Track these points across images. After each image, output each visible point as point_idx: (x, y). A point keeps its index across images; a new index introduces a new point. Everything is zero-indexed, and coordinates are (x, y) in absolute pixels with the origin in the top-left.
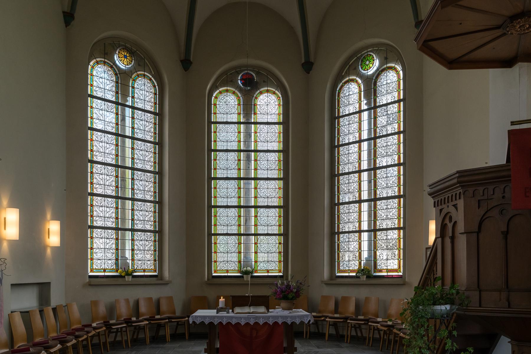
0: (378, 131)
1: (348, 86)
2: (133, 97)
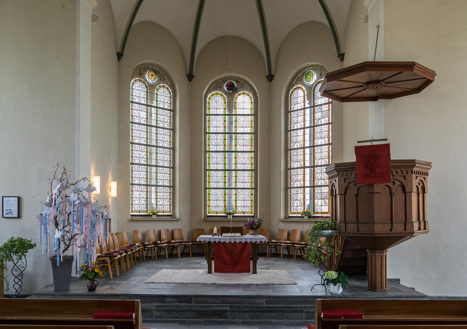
0: (316, 122)
1: (297, 92)
2: (157, 101)
